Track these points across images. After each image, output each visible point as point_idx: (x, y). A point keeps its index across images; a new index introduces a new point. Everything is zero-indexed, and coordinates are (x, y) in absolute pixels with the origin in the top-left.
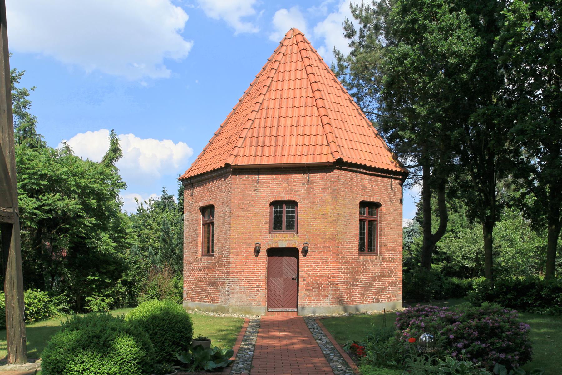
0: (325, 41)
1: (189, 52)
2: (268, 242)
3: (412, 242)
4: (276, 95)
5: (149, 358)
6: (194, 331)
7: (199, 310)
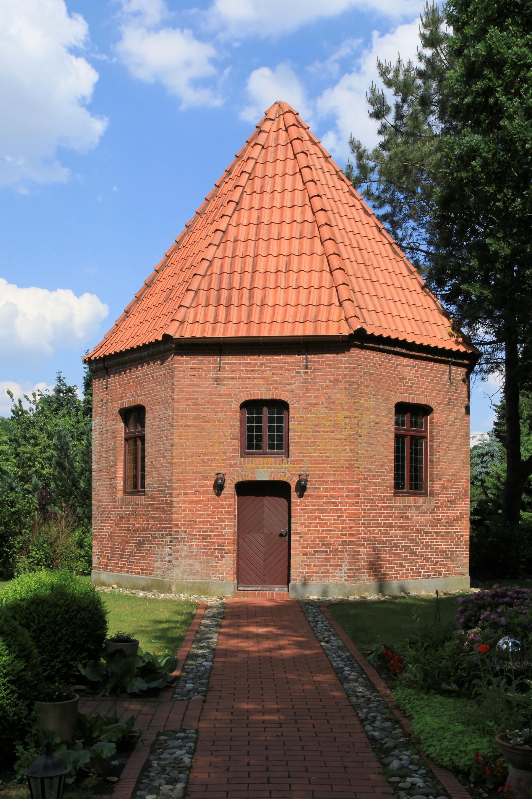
0: (337, 122)
1: (100, 137)
2: (237, 471)
3: (487, 474)
4: (249, 217)
5: (30, 673)
6: (110, 625)
7: (120, 586)
